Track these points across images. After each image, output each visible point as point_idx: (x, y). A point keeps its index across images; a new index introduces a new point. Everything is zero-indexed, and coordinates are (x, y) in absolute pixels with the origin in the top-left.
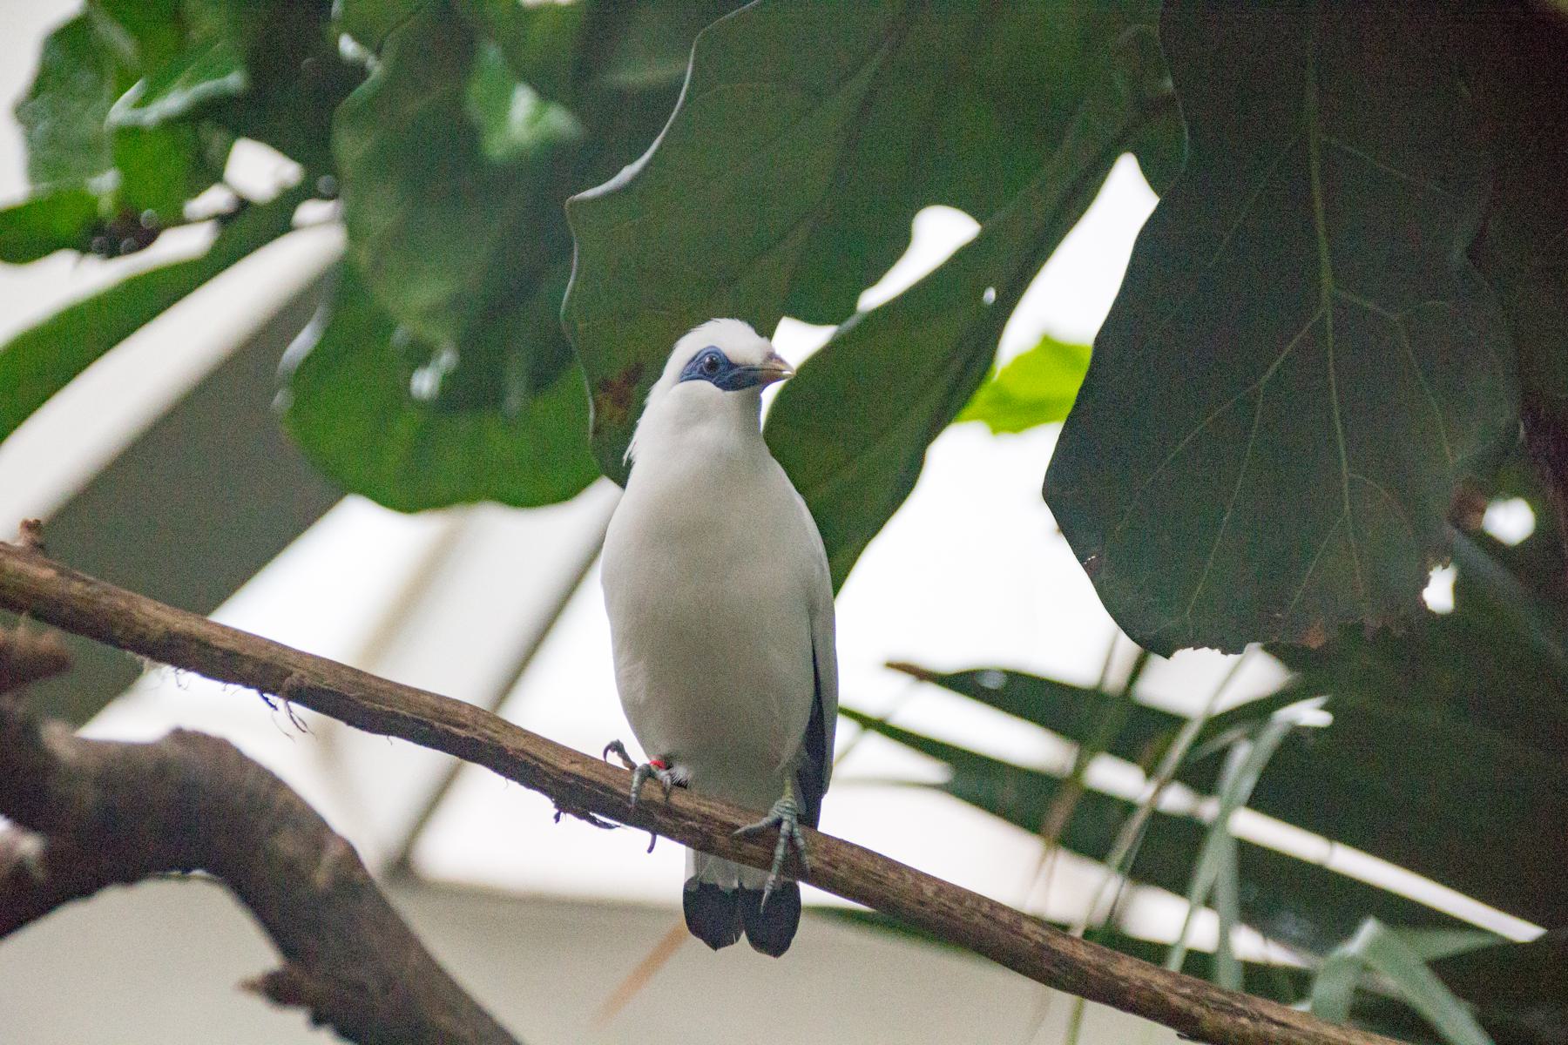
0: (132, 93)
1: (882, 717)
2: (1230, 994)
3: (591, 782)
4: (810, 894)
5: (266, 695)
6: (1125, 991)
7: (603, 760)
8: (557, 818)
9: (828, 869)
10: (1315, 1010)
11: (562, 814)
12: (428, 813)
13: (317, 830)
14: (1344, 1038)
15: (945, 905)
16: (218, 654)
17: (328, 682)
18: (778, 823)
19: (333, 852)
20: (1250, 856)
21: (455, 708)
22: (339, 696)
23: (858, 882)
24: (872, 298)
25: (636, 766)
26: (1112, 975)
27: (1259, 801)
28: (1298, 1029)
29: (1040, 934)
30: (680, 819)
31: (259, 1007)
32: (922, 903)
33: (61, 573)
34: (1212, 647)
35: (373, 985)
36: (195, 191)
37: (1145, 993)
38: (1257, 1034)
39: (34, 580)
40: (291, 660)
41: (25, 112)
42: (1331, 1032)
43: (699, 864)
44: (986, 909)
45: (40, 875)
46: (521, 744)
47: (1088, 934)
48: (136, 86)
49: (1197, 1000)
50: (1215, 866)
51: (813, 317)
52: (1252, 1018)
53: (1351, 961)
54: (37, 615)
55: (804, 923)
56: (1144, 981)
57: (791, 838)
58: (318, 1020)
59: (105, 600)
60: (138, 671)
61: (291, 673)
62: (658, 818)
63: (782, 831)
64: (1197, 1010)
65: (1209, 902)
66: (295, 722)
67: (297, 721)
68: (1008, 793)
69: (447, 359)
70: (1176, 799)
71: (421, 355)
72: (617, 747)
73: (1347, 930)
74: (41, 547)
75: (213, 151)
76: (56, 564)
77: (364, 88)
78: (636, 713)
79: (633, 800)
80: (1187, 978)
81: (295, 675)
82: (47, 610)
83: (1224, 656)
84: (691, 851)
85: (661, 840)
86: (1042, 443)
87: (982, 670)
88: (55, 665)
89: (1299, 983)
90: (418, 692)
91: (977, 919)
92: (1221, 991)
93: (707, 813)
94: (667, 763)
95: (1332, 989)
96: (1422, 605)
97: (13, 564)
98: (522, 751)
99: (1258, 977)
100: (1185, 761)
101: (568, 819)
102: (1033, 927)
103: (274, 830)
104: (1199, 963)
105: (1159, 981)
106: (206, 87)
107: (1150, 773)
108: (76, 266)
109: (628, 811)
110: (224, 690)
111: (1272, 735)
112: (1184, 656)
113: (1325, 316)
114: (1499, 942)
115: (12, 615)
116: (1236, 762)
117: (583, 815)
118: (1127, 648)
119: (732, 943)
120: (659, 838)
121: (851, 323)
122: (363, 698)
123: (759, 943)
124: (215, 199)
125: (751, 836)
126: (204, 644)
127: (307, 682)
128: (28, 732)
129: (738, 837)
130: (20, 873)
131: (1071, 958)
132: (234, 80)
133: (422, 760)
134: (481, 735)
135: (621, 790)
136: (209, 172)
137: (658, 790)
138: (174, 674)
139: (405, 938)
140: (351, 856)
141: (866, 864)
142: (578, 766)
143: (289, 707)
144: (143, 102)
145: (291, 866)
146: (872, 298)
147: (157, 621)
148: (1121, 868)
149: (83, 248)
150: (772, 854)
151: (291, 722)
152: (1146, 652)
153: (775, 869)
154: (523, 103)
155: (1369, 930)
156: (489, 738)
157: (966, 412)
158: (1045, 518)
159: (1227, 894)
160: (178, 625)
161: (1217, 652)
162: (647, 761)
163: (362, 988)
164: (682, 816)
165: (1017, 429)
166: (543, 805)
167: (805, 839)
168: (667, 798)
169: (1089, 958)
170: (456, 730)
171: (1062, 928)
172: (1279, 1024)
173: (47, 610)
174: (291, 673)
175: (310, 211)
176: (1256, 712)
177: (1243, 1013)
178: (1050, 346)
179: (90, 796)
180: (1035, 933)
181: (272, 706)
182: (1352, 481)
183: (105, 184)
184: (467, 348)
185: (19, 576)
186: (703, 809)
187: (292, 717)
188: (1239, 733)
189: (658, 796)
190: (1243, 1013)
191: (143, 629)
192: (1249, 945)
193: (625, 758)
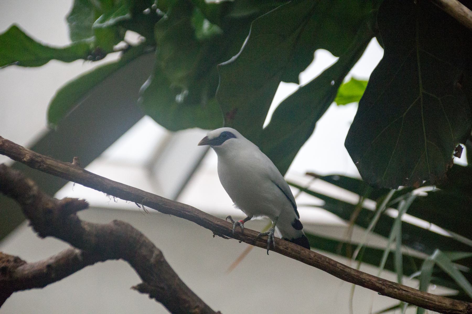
3: (221, 226)
6: (365, 282)
7: (226, 220)
8: (214, 236)
9: (286, 250)
12: (180, 192)
14: (422, 294)
19: (156, 252)
20: (406, 226)
21: (187, 207)
23: (294, 253)
27: (410, 212)
28: (410, 292)
30: (246, 237)
31: (136, 293)
32: (310, 259)
36: (116, 43)
38: (399, 294)
44: (327, 260)
45: (80, 258)
46: (204, 217)
49: (383, 285)
50: (396, 231)
52: (398, 289)
56: (369, 279)
58: (151, 297)
61: (144, 198)
64: (383, 287)
65: (395, 240)
67: (146, 210)
69: (186, 92)
71: (178, 91)
74: (79, 164)
75: (121, 32)
91: (325, 263)
98: (205, 219)
101: (217, 237)
102: (340, 265)
106: (119, 18)
108: (84, 63)
113: (420, 99)
116: (400, 208)
124: (121, 45)
130: (75, 258)
131: (350, 273)
132: (128, 16)
134: (194, 214)
136: (121, 38)
142: (219, 222)
143: (144, 208)
149: (85, 59)
154: (206, 25)
159: (399, 239)
160: (115, 185)
163: (162, 288)
164: (247, 236)
165: (344, 104)
169: (355, 273)
170: (187, 213)
172: (405, 291)
178: (354, 81)
180: (340, 266)
181: (139, 206)
182: (427, 142)
183: (91, 40)
188: (402, 198)
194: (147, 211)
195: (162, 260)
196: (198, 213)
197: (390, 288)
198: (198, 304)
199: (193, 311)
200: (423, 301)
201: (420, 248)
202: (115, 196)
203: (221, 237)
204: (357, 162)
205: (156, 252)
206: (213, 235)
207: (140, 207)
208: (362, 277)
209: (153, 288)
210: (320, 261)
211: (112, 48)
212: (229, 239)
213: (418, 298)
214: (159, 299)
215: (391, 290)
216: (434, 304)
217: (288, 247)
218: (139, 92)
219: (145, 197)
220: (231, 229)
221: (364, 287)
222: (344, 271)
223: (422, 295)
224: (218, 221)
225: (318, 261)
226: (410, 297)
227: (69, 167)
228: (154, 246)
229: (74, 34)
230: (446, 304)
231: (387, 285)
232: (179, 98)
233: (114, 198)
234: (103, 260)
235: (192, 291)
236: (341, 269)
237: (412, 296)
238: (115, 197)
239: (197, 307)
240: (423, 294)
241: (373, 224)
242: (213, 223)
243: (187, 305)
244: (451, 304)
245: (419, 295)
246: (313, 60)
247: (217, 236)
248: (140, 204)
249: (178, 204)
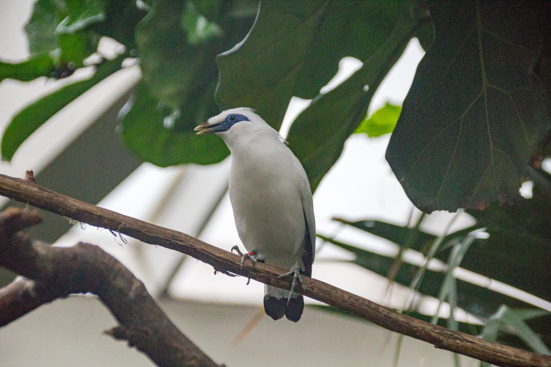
0: (64, 21)
1: (331, 238)
2: (453, 332)
3: (226, 260)
4: (307, 300)
5: (112, 231)
6: (417, 331)
7: (231, 252)
8: (215, 273)
10: (484, 338)
11: (217, 271)
13: (130, 278)
14: (493, 347)
15: (352, 302)
16: (95, 217)
17: (135, 227)
18: (293, 274)
19: (136, 285)
20: (461, 284)
22: (138, 231)
23: (321, 294)
24: (325, 89)
25: (243, 254)
26: (411, 325)
27: (465, 264)
28: (477, 344)
29: (386, 312)
32: (344, 301)
33: (40, 189)
34: (446, 210)
35: (150, 332)
37: (423, 332)
38: (462, 346)
39: (32, 192)
40: (121, 219)
41: (28, 28)
42: (489, 345)
43: (269, 290)
44: (366, 303)
46: (203, 247)
47: (404, 312)
48: (66, 18)
49: (442, 334)
50: (448, 288)
51: (304, 97)
52: (460, 340)
53: (497, 321)
54: (32, 204)
55: (305, 311)
56: (423, 328)
57: (298, 279)
58: (131, 344)
59: (56, 198)
60: (72, 225)
62: (251, 272)
63: (294, 277)
64: (441, 337)
65: (446, 300)
66: (123, 241)
68: (376, 263)
69: (176, 113)
70: (435, 265)
71: (167, 112)
72: (236, 248)
73: (495, 310)
76: (39, 186)
77: (146, 18)
78: (243, 237)
79: (242, 266)
80: (438, 327)
81: (122, 224)
82: (34, 202)
83: (450, 213)
84: (266, 285)
85: (252, 280)
86: (384, 141)
87: (366, 221)
88: (38, 221)
89: (478, 329)
90: (166, 229)
91: (364, 307)
92: (450, 331)
93: (268, 271)
94: (254, 253)
95: (490, 331)
96: (519, 195)
97: (24, 186)
99: (464, 327)
100: (438, 250)
101: (219, 274)
102: (383, 309)
103: (115, 278)
104: (443, 322)
105: (428, 328)
106: (91, 19)
107: (425, 255)
109: (240, 270)
110: (98, 230)
111: (468, 241)
112: (436, 213)
114: (545, 314)
115: (25, 204)
117: (224, 272)
118: (417, 212)
119: (281, 318)
120: (251, 279)
121: (317, 98)
122: (146, 231)
123: (290, 318)
124: (94, 58)
125: (284, 278)
126: (91, 214)
127: (127, 226)
128: (28, 244)
129: (279, 279)
130: (26, 294)
132: (100, 16)
133: (170, 255)
135: (238, 263)
136: (92, 49)
137: (251, 263)
138: (80, 224)
139: (162, 315)
140: (142, 286)
141: (324, 288)
142: (222, 255)
143: (121, 237)
144: (68, 24)
145: (121, 290)
146: (325, 89)
147: (74, 205)
148: (415, 289)
150: (291, 285)
151: (121, 240)
152: (424, 213)
153: (292, 290)
154: (201, 24)
155: (503, 310)
156: (191, 245)
157: (358, 130)
158: (386, 167)
161: (447, 212)
162: (247, 252)
163: (146, 333)
166: (210, 268)
167: (302, 279)
168: (254, 265)
169: (403, 320)
171: (394, 311)
173: (34, 202)
174: (121, 223)
175: (128, 62)
176: (462, 234)
177: (458, 338)
179: (50, 267)
181: (114, 235)
183: (56, 54)
184: (183, 109)
185: (25, 190)
186: (266, 269)
187: (122, 239)
189: (251, 265)
190: (458, 338)
191: (69, 208)
192: (461, 316)
193: (239, 251)
195: (145, 294)
198: (194, 353)
199: (188, 363)
201: (478, 311)
202: (82, 222)
203: (225, 274)
204: (402, 178)
206: (214, 272)
207: (116, 235)
208: (412, 325)
209: (133, 332)
210: (357, 304)
212: (235, 276)
213: (488, 351)
214: (141, 349)
215: (451, 341)
219: (122, 222)
222: (389, 317)
224: (220, 253)
225: (354, 304)
227: (19, 183)
228: (132, 276)
230: (524, 359)
231: (447, 335)
232: (168, 122)
233: (81, 224)
236: (385, 315)
239: (194, 357)
240: (495, 346)
241: (415, 282)
244: (532, 359)
246: (336, 75)
247: (219, 272)
248: (116, 232)
249: (167, 231)
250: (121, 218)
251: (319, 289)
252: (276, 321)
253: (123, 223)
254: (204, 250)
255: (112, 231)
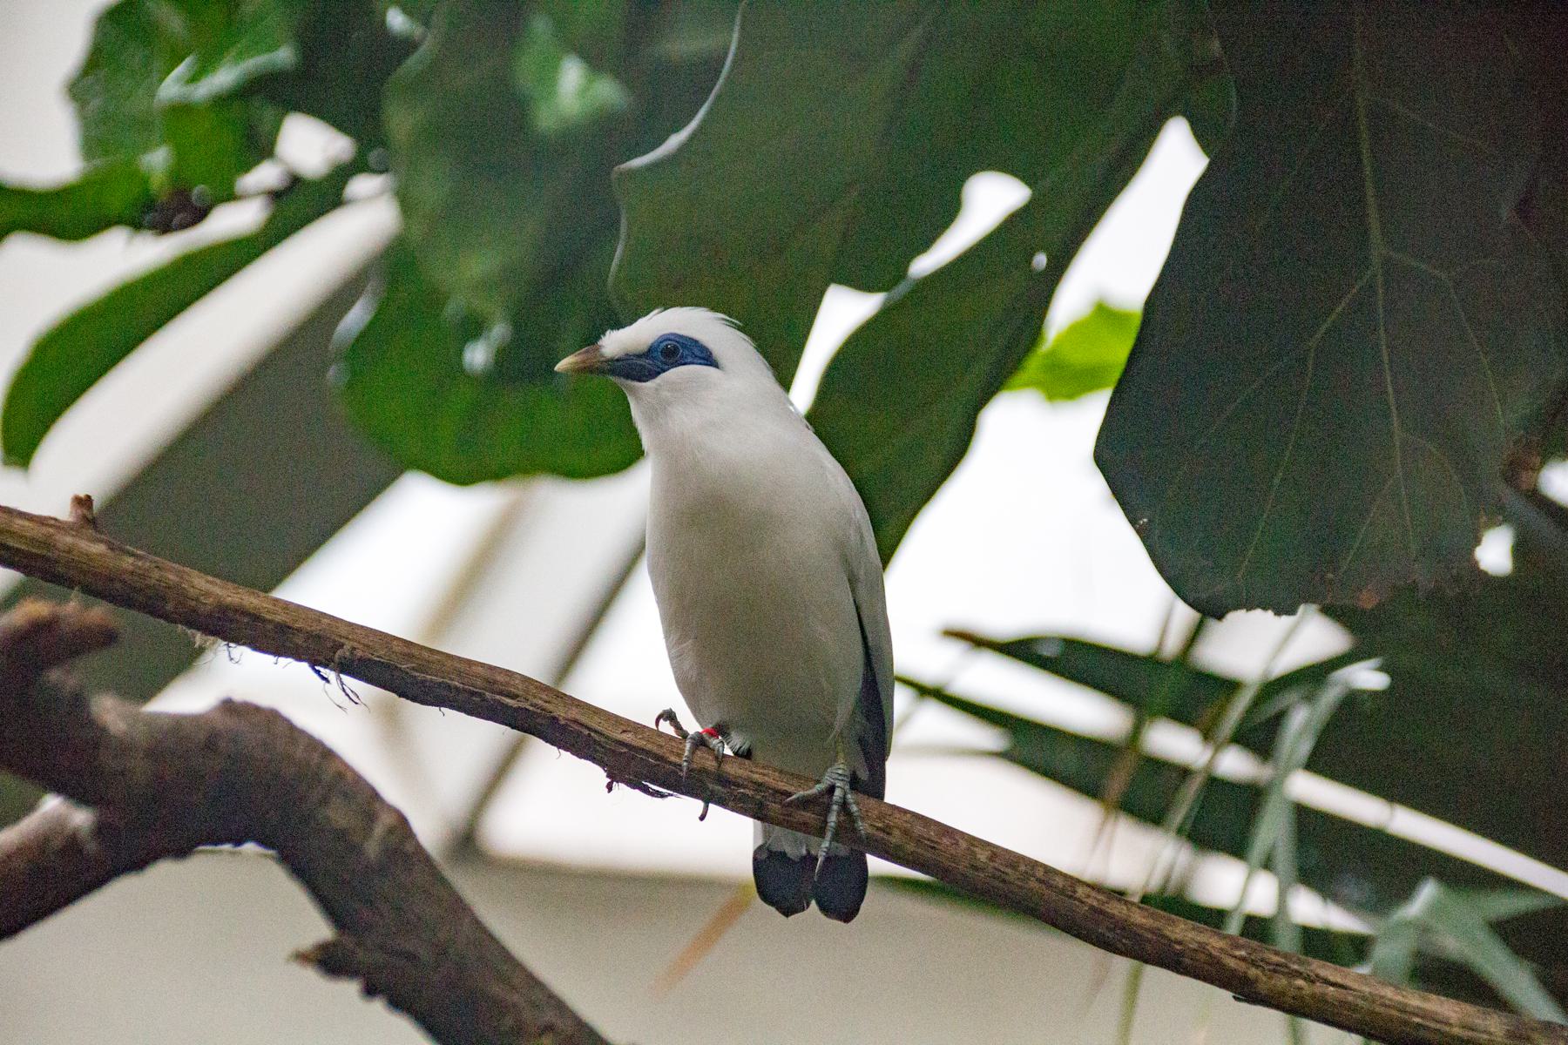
5: (317, 668)
6: (1181, 954)
7: (655, 728)
8: (610, 788)
11: (615, 783)
14: (1399, 998)
18: (831, 789)
20: (1308, 820)
23: (911, 847)
27: (1318, 763)
28: (1355, 990)
31: (311, 976)
36: (247, 167)
38: (1313, 996)
44: (1040, 873)
46: (574, 713)
49: (1254, 963)
50: (1272, 830)
52: (1307, 979)
57: (844, 805)
58: (370, 991)
64: (1253, 972)
65: (1268, 865)
69: (499, 331)
71: (473, 328)
91: (1033, 884)
101: (621, 789)
119: (803, 910)
124: (265, 175)
130: (72, 844)
132: (284, 56)
136: (260, 147)
142: (630, 735)
143: (342, 684)
149: (137, 225)
163: (412, 957)
169: (1144, 921)
180: (1089, 896)
183: (157, 161)
194: (356, 694)
196: (546, 702)
197: (1281, 976)
198: (549, 1016)
200: (1406, 1023)
205: (386, 820)
206: (606, 784)
208: (1173, 937)
211: (230, 184)
212: (667, 796)
213: (1382, 1010)
214: (398, 1003)
215: (1281, 982)
216: (1445, 1035)
217: (888, 826)
218: (335, 336)
220: (673, 759)
221: (1178, 972)
222: (1101, 912)
223: (1400, 1003)
226: (1354, 1008)
228: (375, 796)
229: (94, 142)
230: (1490, 1033)
232: (477, 356)
234: (182, 851)
235: (530, 969)
236: (1092, 907)
237: (1360, 1002)
238: (231, 644)
242: (607, 737)
243: (509, 1021)
245: (1387, 1002)
247: (622, 785)
250: (343, 631)
251: (906, 832)
252: (790, 918)
253: (348, 646)
254: (576, 721)
255: (317, 668)
